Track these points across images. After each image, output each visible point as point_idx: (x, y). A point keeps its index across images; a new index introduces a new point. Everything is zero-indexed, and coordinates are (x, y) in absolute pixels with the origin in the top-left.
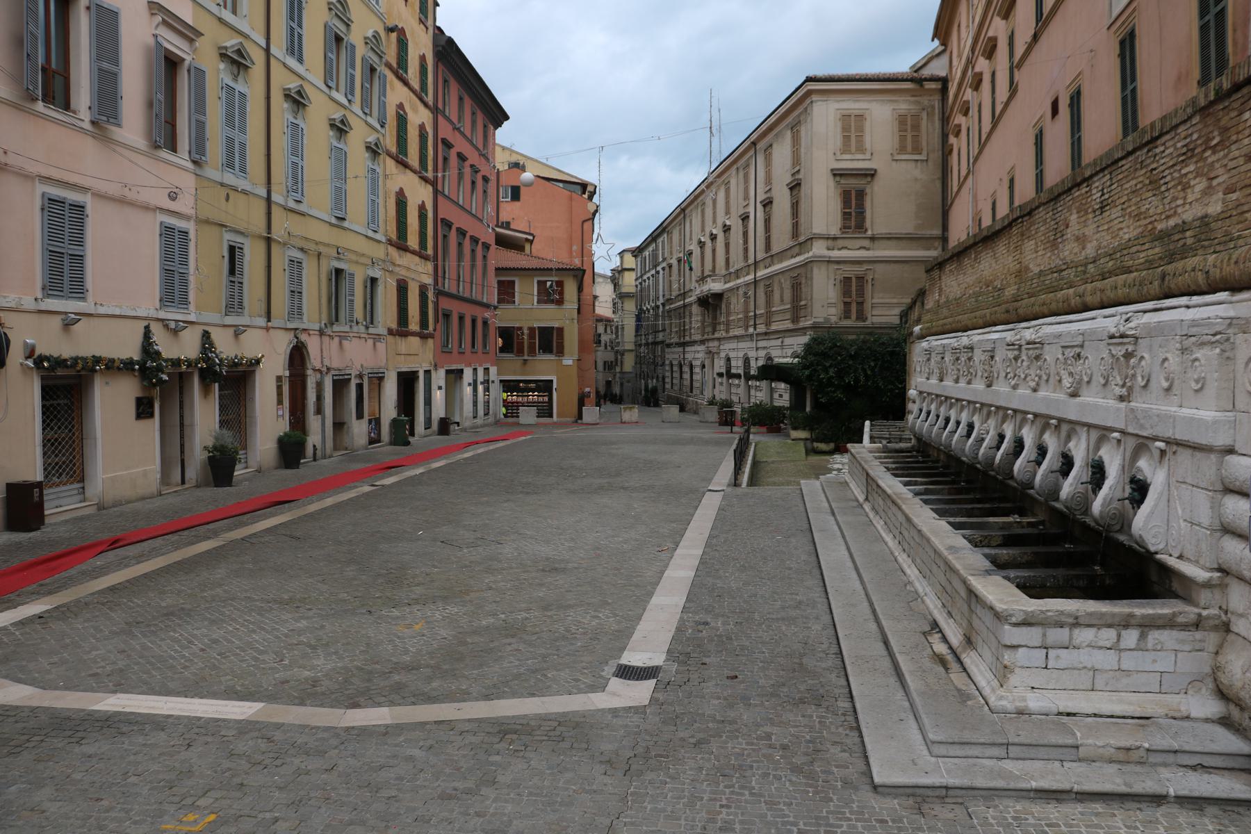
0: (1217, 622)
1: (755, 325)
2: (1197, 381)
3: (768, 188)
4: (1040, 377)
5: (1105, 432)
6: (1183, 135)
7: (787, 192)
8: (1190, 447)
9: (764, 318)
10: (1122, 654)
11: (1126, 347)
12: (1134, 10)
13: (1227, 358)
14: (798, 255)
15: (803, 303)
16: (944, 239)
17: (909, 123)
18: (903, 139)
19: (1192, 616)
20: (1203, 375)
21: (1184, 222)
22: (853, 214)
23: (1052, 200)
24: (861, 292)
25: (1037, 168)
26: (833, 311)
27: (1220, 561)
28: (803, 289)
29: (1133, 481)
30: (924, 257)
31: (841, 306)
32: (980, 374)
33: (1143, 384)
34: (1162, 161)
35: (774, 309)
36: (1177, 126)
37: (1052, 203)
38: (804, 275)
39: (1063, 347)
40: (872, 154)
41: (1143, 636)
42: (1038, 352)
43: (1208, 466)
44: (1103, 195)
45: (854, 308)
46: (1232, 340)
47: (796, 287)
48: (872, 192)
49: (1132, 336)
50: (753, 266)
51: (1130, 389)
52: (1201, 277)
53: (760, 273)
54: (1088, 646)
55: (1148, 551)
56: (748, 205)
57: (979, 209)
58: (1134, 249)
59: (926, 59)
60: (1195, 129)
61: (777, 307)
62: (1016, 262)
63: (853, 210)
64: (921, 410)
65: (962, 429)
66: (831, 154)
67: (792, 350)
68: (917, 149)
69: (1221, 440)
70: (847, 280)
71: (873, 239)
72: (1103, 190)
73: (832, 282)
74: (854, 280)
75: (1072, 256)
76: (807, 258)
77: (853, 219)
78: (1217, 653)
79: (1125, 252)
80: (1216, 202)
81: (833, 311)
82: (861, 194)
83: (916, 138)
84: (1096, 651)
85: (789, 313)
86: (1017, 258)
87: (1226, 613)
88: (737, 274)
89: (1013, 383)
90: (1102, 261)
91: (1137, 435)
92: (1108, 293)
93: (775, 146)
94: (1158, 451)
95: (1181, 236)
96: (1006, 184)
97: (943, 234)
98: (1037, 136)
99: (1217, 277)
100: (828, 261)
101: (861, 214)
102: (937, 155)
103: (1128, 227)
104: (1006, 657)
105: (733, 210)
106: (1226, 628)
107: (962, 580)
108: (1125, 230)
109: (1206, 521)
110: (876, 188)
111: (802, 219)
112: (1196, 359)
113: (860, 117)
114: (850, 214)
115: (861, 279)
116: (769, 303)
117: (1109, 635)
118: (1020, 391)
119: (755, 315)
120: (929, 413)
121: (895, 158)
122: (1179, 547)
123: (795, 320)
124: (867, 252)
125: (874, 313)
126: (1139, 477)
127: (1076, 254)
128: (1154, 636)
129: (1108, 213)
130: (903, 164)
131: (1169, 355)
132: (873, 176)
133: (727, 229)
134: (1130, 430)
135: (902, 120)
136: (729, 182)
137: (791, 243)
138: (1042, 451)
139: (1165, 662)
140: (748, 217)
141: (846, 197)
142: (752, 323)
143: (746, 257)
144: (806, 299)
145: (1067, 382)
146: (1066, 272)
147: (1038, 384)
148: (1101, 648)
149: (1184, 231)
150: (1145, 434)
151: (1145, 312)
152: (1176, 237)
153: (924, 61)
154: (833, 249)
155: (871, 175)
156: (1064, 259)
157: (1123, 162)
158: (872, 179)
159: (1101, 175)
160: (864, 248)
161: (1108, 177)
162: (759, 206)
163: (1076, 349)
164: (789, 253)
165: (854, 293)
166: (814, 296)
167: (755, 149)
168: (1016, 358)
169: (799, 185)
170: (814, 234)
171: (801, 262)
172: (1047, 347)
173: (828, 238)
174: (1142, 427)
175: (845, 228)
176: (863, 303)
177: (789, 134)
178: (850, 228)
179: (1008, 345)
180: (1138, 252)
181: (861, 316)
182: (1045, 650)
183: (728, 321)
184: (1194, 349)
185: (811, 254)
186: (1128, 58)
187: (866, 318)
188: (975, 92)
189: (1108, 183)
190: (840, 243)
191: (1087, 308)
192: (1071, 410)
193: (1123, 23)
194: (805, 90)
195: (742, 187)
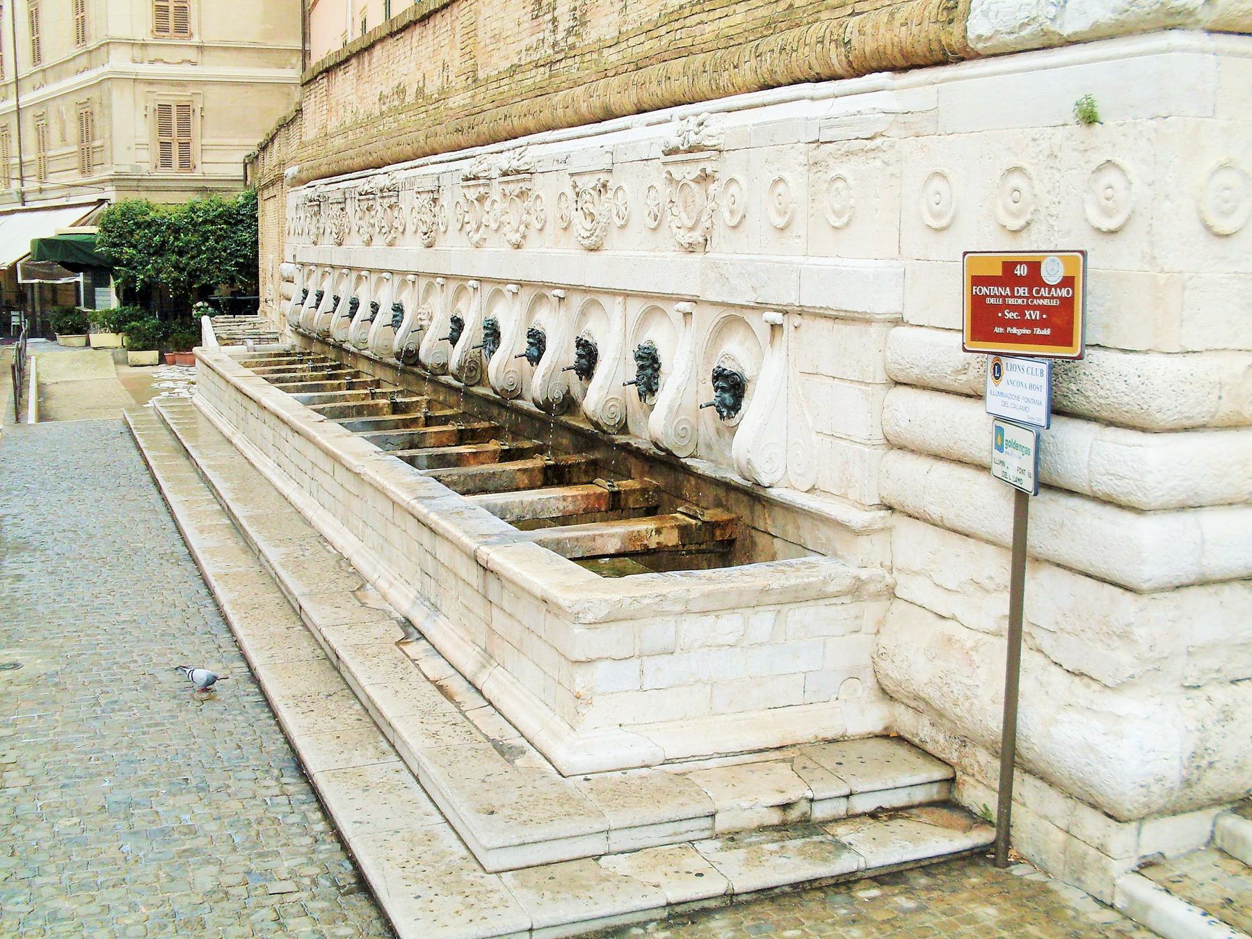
0: (880, 586)
1: (22, 179)
2: (838, 214)
9: (36, 167)
11: (701, 166)
14: (87, 69)
15: (97, 143)
16: (305, 54)
20: (852, 202)
22: (171, 9)
24: (185, 128)
27: (884, 494)
28: (97, 123)
29: (719, 375)
32: (410, 229)
33: (735, 222)
35: (50, 153)
39: (572, 175)
46: (897, 148)
47: (86, 120)
50: (13, 88)
58: (696, 19)
62: (467, 57)
64: (306, 292)
65: (385, 315)
69: (886, 305)
70: (164, 109)
71: (200, 48)
76: (103, 74)
81: (144, 155)
85: (76, 159)
86: (468, 50)
89: (476, 237)
90: (631, 42)
92: (654, 87)
99: (867, 50)
104: (578, 680)
106: (891, 593)
107: (469, 556)
114: (166, 9)
115: (184, 109)
116: (42, 144)
118: (488, 249)
119: (21, 163)
120: (320, 296)
123: (86, 169)
126: (730, 367)
131: (785, 175)
138: (537, 342)
142: (16, 174)
144: (102, 137)
146: (563, 64)
163: (598, 176)
164: (71, 66)
171: (91, 80)
175: (161, 29)
178: (166, 30)
179: (467, 179)
180: (702, 23)
181: (186, 163)
184: (831, 161)
185: (107, 68)
190: (153, 53)
192: (593, 271)
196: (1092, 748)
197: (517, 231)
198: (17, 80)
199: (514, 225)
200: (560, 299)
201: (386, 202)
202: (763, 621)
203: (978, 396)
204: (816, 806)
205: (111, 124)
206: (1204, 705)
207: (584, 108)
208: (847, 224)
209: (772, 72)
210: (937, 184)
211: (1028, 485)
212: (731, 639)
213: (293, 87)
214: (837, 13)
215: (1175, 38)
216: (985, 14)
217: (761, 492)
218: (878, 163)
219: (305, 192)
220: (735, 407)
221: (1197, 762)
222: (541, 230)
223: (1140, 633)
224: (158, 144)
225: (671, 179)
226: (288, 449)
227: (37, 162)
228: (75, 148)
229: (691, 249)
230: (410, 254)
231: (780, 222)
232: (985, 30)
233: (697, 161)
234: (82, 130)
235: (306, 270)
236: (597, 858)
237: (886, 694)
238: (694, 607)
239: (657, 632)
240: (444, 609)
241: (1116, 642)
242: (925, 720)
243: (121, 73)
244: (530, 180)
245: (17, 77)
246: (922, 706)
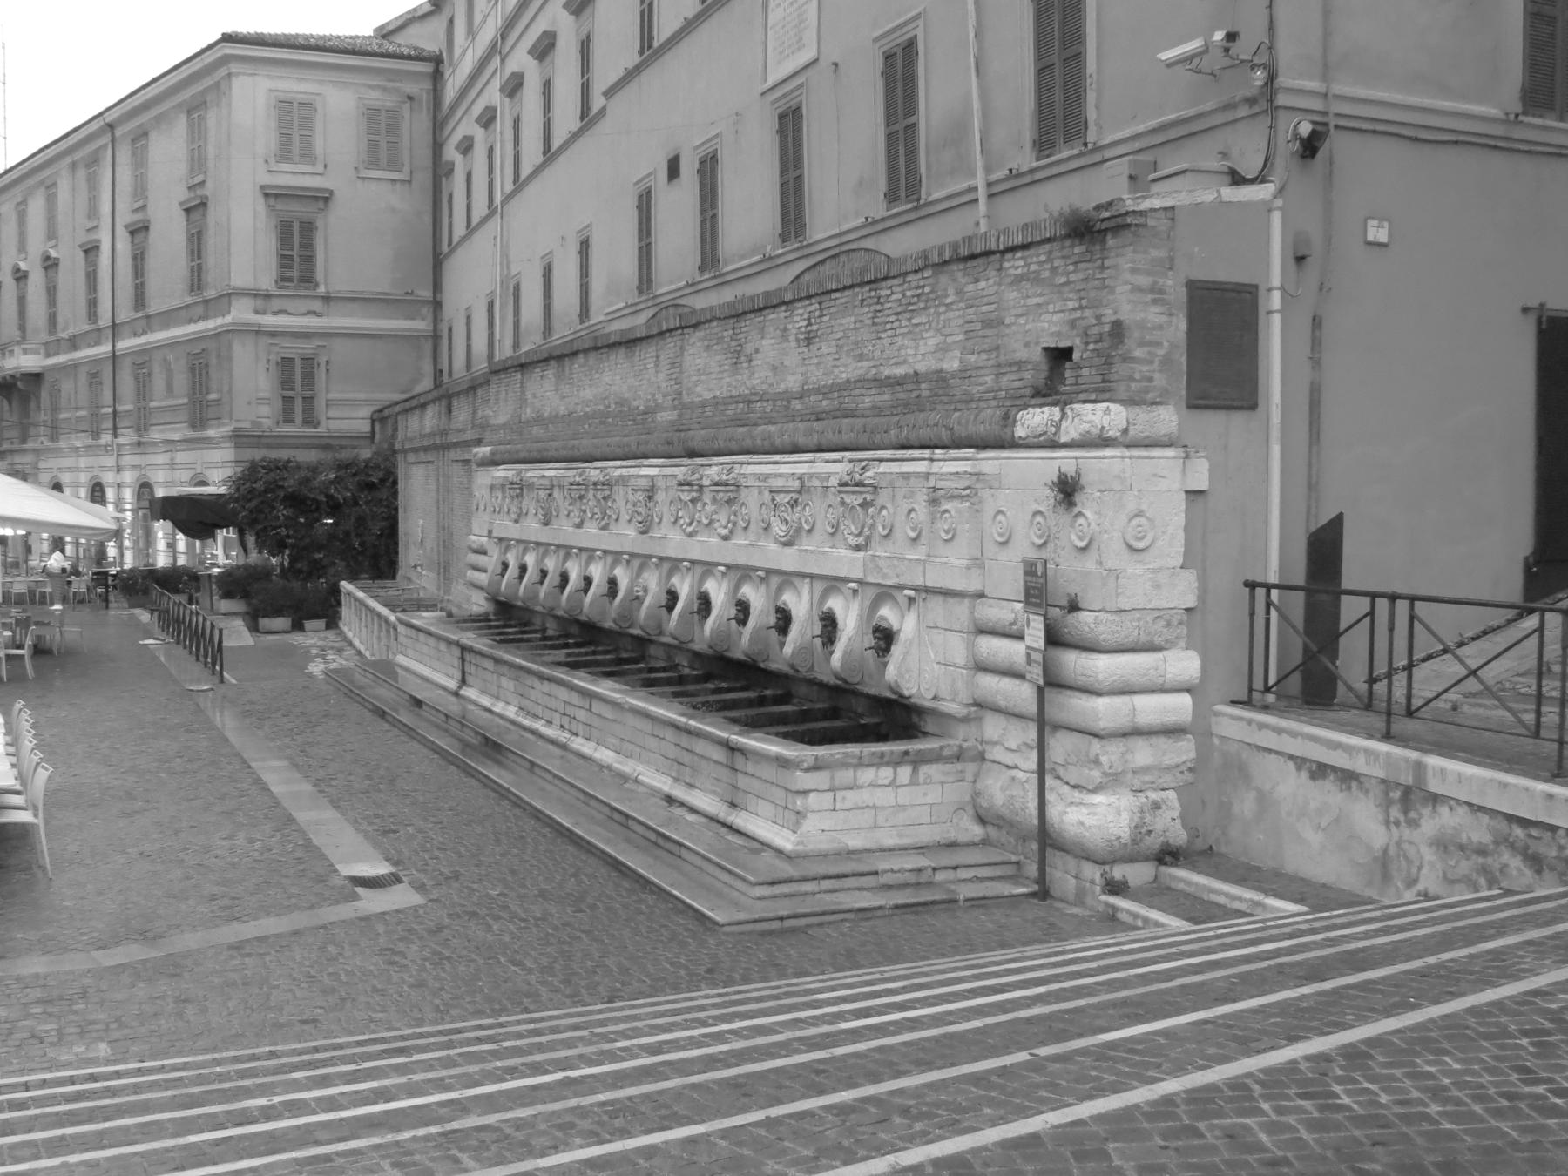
2: (947, 532)
3: (140, 204)
5: (833, 583)
6: (914, 284)
7: (180, 218)
8: (941, 593)
10: (899, 790)
12: (801, 86)
13: (977, 511)
15: (213, 396)
18: (373, 147)
21: (916, 373)
22: (297, 259)
23: (733, 316)
24: (309, 379)
26: (265, 410)
31: (279, 403)
34: (889, 305)
35: (153, 404)
40: (325, 166)
41: (915, 771)
42: (732, 495)
43: (961, 609)
50: (109, 332)
51: (868, 539)
53: (125, 344)
57: (514, 272)
58: (857, 392)
59: (403, 20)
63: (295, 253)
66: (261, 161)
68: (394, 164)
70: (286, 363)
71: (327, 299)
72: (809, 319)
74: (298, 362)
78: (975, 781)
79: (845, 393)
81: (265, 410)
82: (308, 228)
83: (394, 147)
86: (674, 376)
87: (981, 744)
88: (74, 343)
89: (690, 529)
92: (830, 436)
93: (153, 136)
94: (906, 600)
100: (257, 332)
101: (308, 260)
102: (424, 178)
106: (981, 757)
108: (842, 369)
109: (961, 661)
111: (211, 260)
112: (946, 511)
113: (308, 106)
115: (309, 361)
117: (886, 773)
119: (115, 413)
124: (319, 319)
125: (331, 414)
126: (884, 624)
127: (772, 385)
128: (924, 769)
130: (373, 186)
131: (916, 507)
132: (326, 200)
133: (50, 264)
134: (871, 579)
135: (372, 116)
137: (189, 300)
139: (933, 795)
140: (97, 248)
141: (284, 233)
143: (92, 314)
147: (731, 532)
150: (889, 582)
151: (881, 460)
152: (910, 387)
153: (399, 23)
154: (264, 314)
155: (324, 198)
156: (754, 388)
159: (807, 302)
161: (817, 306)
168: (693, 501)
169: (203, 204)
170: (234, 288)
173: (256, 296)
174: (885, 576)
175: (283, 279)
176: (312, 398)
177: (181, 124)
178: (290, 280)
181: (310, 420)
182: (832, 794)
183: (55, 420)
185: (228, 319)
187: (319, 423)
188: (507, 100)
189: (817, 313)
190: (276, 304)
192: (788, 560)
193: (785, 96)
194: (219, 54)
197: (725, 527)
199: (724, 522)
201: (600, 495)
202: (905, 772)
203: (1021, 637)
204: (937, 873)
205: (231, 376)
206: (1144, 800)
207: (778, 442)
210: (1000, 517)
211: (1041, 682)
214: (947, 407)
215: (1108, 452)
216: (1023, 425)
217: (906, 702)
218: (968, 504)
219: (500, 473)
220: (887, 650)
221: (1139, 829)
223: (1104, 759)
224: (280, 400)
225: (843, 503)
226: (533, 694)
229: (857, 548)
230: (626, 536)
231: (913, 535)
233: (861, 493)
234: (194, 382)
235: (504, 544)
236: (814, 894)
237: (982, 821)
239: (845, 776)
240: (698, 785)
241: (1092, 766)
243: (244, 324)
244: (737, 491)
245: (113, 321)
246: (1001, 823)
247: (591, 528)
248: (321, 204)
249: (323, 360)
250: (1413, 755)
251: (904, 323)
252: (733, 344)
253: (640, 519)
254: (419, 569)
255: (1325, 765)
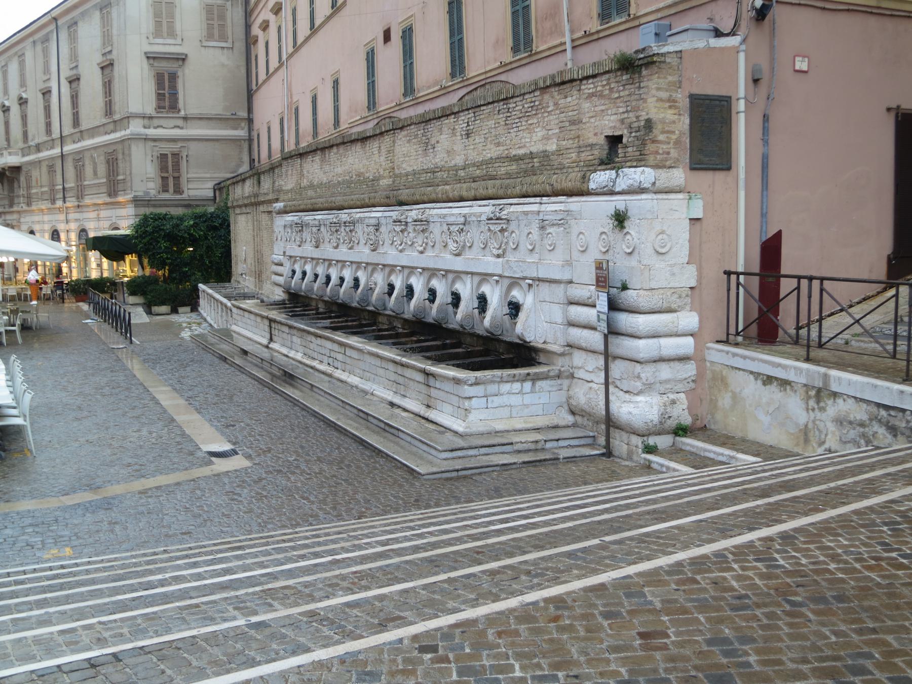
0: (568, 373)
2: (550, 245)
3: (74, 65)
4: (427, 244)
6: (529, 100)
15: (121, 177)
17: (216, 12)
18: (210, 27)
19: (557, 371)
21: (531, 153)
22: (167, 95)
23: (423, 122)
24: (177, 167)
25: (368, 79)
28: (121, 165)
30: (232, 136)
32: (363, 242)
33: (514, 247)
35: (86, 183)
36: (524, 94)
37: (423, 124)
38: (121, 151)
40: (182, 40)
41: (533, 384)
43: (559, 290)
44: (468, 125)
45: (171, 182)
47: (112, 163)
48: (184, 75)
49: (505, 219)
52: (548, 188)
53: (68, 148)
54: (508, 393)
55: (525, 342)
56: (49, 79)
57: (295, 100)
60: (537, 99)
61: (89, 181)
63: (166, 92)
64: (294, 272)
67: (110, 222)
68: (223, 37)
70: (163, 157)
71: (185, 119)
72: (468, 123)
73: (149, 158)
74: (170, 156)
75: (443, 163)
76: (125, 136)
77: (167, 99)
80: (552, 144)
81: (151, 185)
82: (173, 77)
83: (222, 27)
84: (511, 395)
85: (106, 187)
88: (38, 148)
89: (400, 248)
91: (511, 277)
93: (80, 24)
94: (527, 286)
95: (530, 161)
96: (329, 85)
97: (249, 116)
98: (368, 53)
100: (145, 139)
101: (174, 96)
102: (240, 45)
103: (490, 149)
105: (30, 81)
106: (572, 376)
109: (560, 321)
110: (187, 71)
111: (117, 97)
114: (164, 95)
115: (176, 156)
117: (517, 386)
119: (64, 188)
121: (204, 44)
122: (544, 337)
124: (181, 131)
125: (190, 186)
126: (514, 300)
128: (539, 384)
129: (473, 138)
130: (211, 50)
131: (532, 231)
132: (184, 60)
134: (506, 274)
136: (23, 54)
137: (104, 121)
139: (544, 398)
140: (50, 91)
141: (159, 79)
143: (49, 130)
145: (452, 246)
148: (513, 393)
149: (532, 158)
150: (517, 276)
151: (511, 204)
152: (527, 161)
155: (182, 59)
156: (436, 163)
157: (484, 108)
158: (183, 63)
159: (467, 112)
160: (178, 127)
162: (63, 81)
164: (102, 129)
165: (170, 168)
166: (134, 171)
167: (57, 24)
170: (131, 113)
172: (432, 225)
174: (515, 272)
175: (159, 108)
177: (97, 15)
178: (164, 108)
181: (178, 190)
184: (547, 227)
185: (128, 132)
186: (455, 16)
189: (473, 119)
190: (156, 122)
191: (462, 199)
192: (458, 264)
195: (40, 60)
196: (630, 413)
198: (61, 137)
199: (420, 243)
200: (443, 275)
201: (348, 229)
202: (528, 385)
205: (131, 166)
207: (451, 195)
208: (553, 249)
209: (527, 191)
212: (517, 391)
213: (243, 142)
214: (549, 172)
215: (644, 196)
216: (594, 182)
217: (528, 345)
218: (562, 229)
219: (290, 218)
220: (516, 315)
222: (433, 246)
223: (642, 375)
225: (489, 230)
227: (76, 188)
228: (105, 180)
229: (498, 256)
230: (363, 253)
231: (530, 247)
232: (594, 187)
233: (500, 224)
234: (109, 169)
235: (293, 260)
237: (573, 413)
238: (505, 379)
239: (492, 388)
242: (585, 419)
246: (584, 414)
247: (343, 249)
248: (180, 63)
249: (184, 154)
250: (823, 370)
251: (524, 123)
252: (424, 138)
253: (371, 243)
254: (244, 276)
255: (772, 377)
